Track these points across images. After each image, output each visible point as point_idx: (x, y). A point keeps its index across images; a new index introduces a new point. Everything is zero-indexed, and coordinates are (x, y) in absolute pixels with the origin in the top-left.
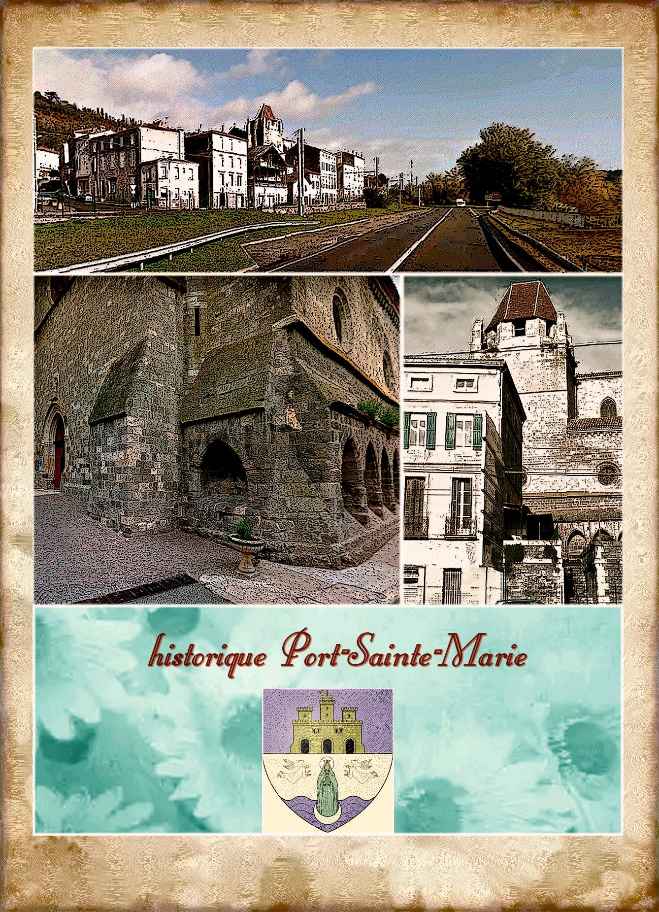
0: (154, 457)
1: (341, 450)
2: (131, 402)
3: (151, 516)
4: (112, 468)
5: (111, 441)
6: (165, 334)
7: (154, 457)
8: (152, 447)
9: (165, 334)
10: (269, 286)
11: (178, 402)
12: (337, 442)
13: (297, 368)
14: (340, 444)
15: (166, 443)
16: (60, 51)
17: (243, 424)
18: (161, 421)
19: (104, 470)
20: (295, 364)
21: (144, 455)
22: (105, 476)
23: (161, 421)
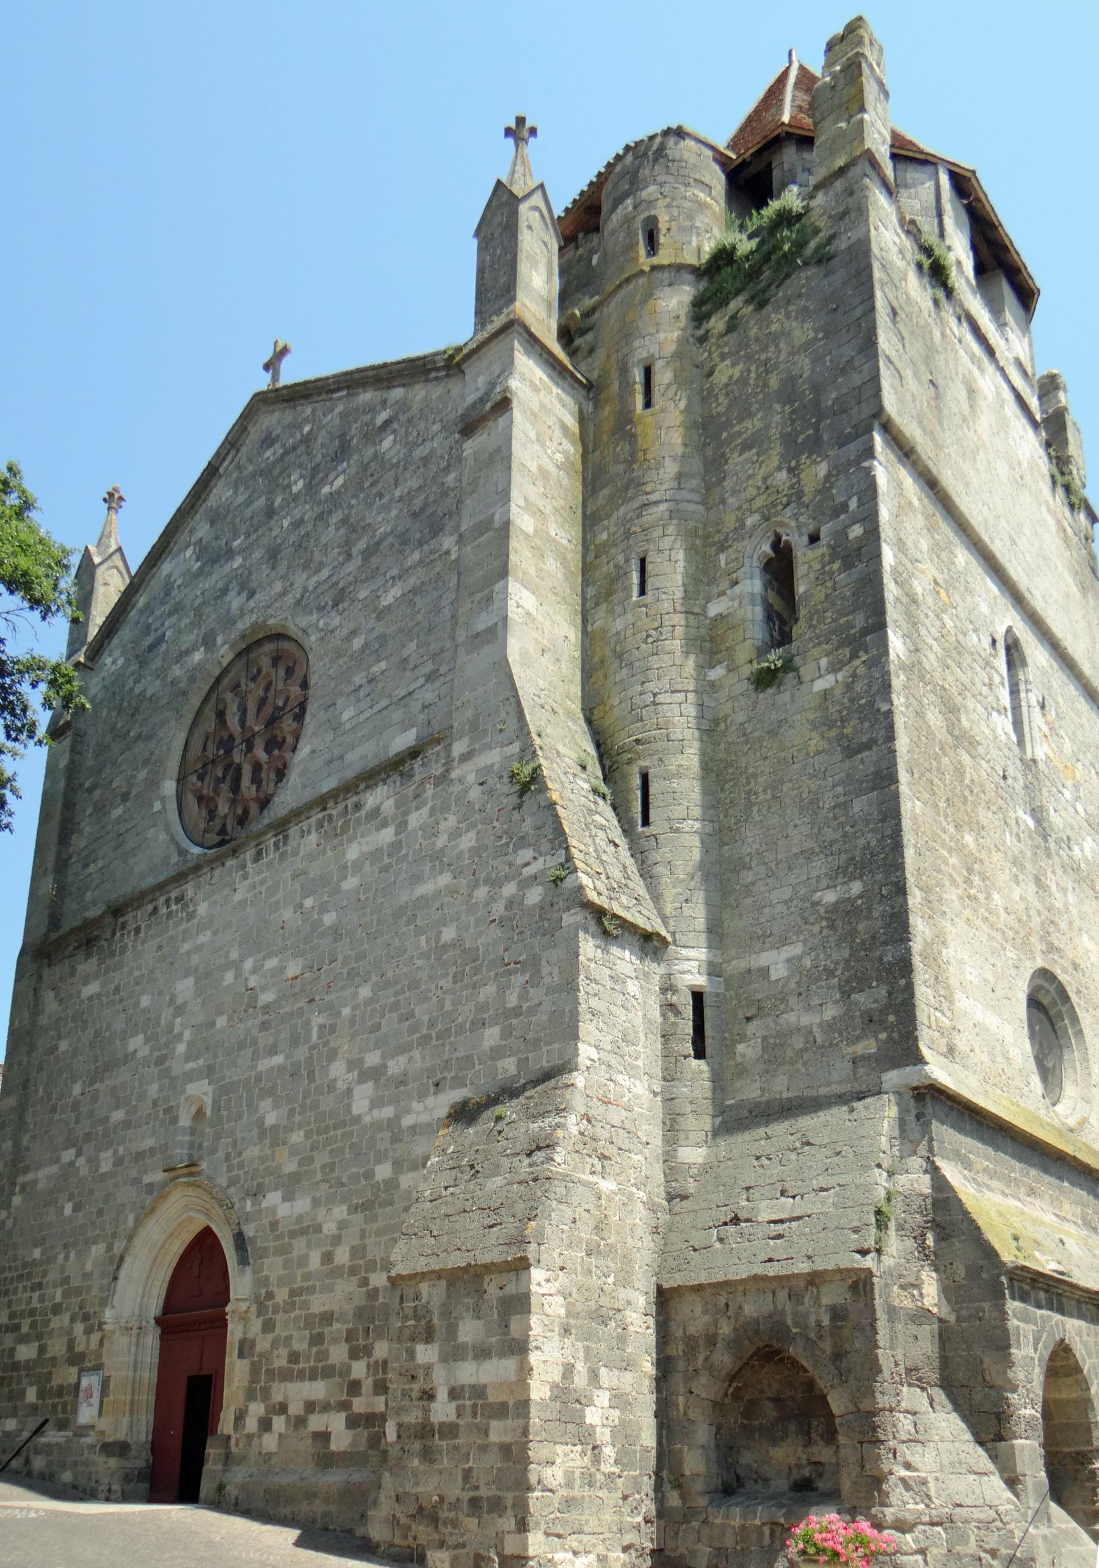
0: (594, 1375)
1: (1037, 1370)
2: (540, 1232)
3: (585, 1538)
4: (475, 1406)
5: (469, 1331)
6: (617, 1052)
7: (594, 1375)
8: (587, 1350)
9: (617, 1052)
10: (870, 987)
11: (655, 1231)
12: (1030, 1351)
13: (940, 1183)
14: (1036, 1356)
15: (622, 1339)
16: (917, 1470)
17: (826, 1300)
18: (611, 1280)
19: (442, 1410)
20: (934, 1171)
21: (568, 1370)
22: (450, 1430)
23: (611, 1280)
